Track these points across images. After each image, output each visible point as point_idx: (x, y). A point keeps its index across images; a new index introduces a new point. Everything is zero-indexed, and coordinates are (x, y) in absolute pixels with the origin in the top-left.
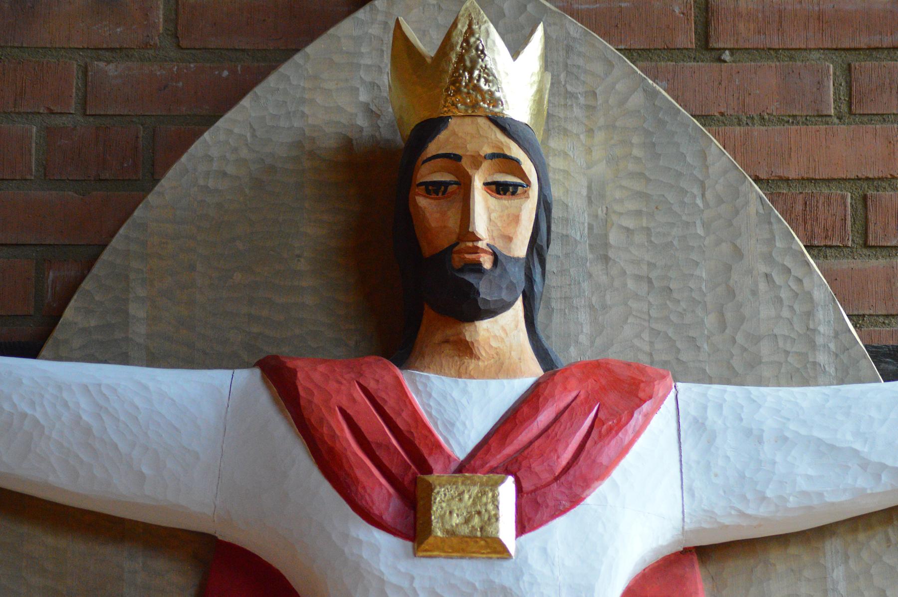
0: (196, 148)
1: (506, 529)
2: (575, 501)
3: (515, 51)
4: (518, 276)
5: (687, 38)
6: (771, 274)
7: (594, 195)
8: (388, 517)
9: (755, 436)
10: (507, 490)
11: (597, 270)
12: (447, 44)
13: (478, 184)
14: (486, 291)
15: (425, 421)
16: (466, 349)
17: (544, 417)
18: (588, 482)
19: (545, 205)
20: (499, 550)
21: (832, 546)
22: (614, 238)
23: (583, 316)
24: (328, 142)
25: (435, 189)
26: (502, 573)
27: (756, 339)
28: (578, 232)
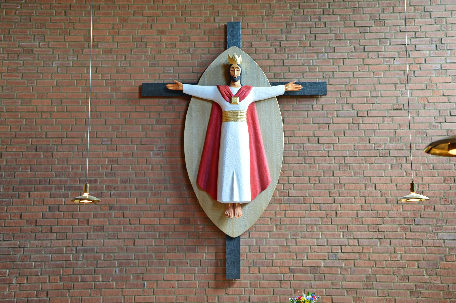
0: (211, 64)
1: (238, 102)
2: (244, 99)
3: (239, 57)
4: (239, 78)
5: (254, 52)
6: (180, 223)
7: (246, 69)
8: (228, 101)
9: (259, 92)
10: (238, 98)
11: (246, 76)
12: (233, 57)
13: (236, 70)
14: (236, 80)
15: (265, 178)
16: (235, 85)
17: (241, 91)
18: (246, 96)
19: (241, 71)
20: (237, 104)
21: (266, 101)
22: (248, 73)
23: (245, 80)
24: (222, 64)
25: (232, 70)
26: (238, 106)
27: (260, 82)
28: (244, 72)
